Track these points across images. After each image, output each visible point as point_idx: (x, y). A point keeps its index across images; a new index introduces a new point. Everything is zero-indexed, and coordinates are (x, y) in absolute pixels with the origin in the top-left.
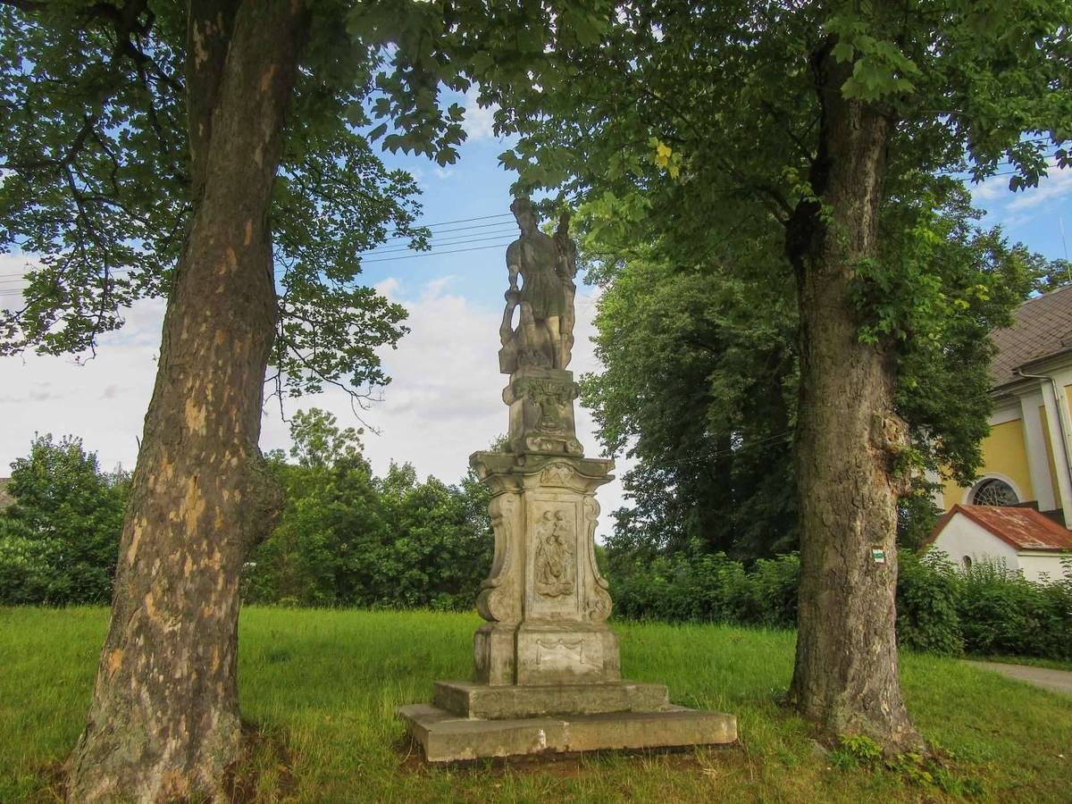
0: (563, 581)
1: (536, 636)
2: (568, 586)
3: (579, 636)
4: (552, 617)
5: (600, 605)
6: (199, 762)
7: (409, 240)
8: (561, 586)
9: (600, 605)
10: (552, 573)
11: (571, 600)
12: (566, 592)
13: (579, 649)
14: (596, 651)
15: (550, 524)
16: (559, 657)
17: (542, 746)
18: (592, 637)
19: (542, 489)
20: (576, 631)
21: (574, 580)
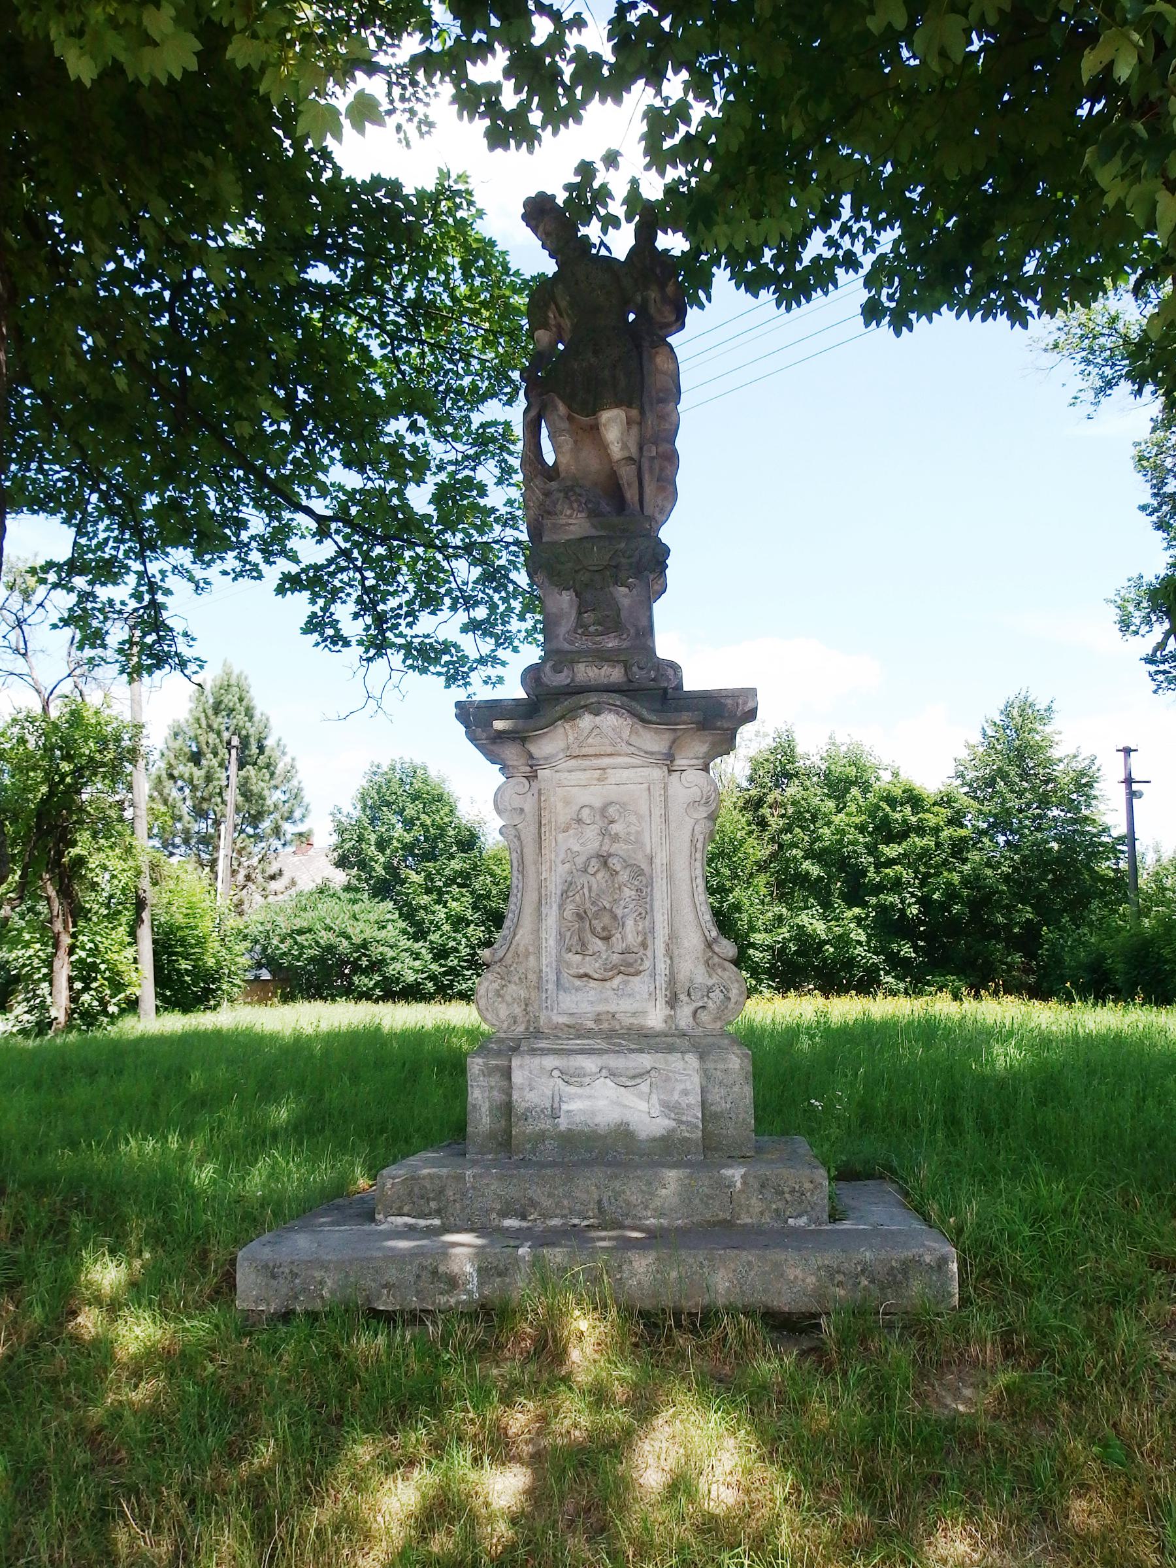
0: (620, 946)
1: (550, 1062)
2: (630, 958)
3: (645, 1061)
4: (597, 1020)
5: (717, 995)
6: (555, 1116)
7: (274, 373)
8: (616, 958)
9: (717, 995)
10: (593, 932)
11: (640, 985)
12: (627, 967)
13: (644, 1087)
14: (685, 1093)
15: (591, 833)
16: (601, 1103)
17: (469, 1293)
18: (675, 1062)
19: (573, 762)
20: (641, 1051)
21: (644, 945)
